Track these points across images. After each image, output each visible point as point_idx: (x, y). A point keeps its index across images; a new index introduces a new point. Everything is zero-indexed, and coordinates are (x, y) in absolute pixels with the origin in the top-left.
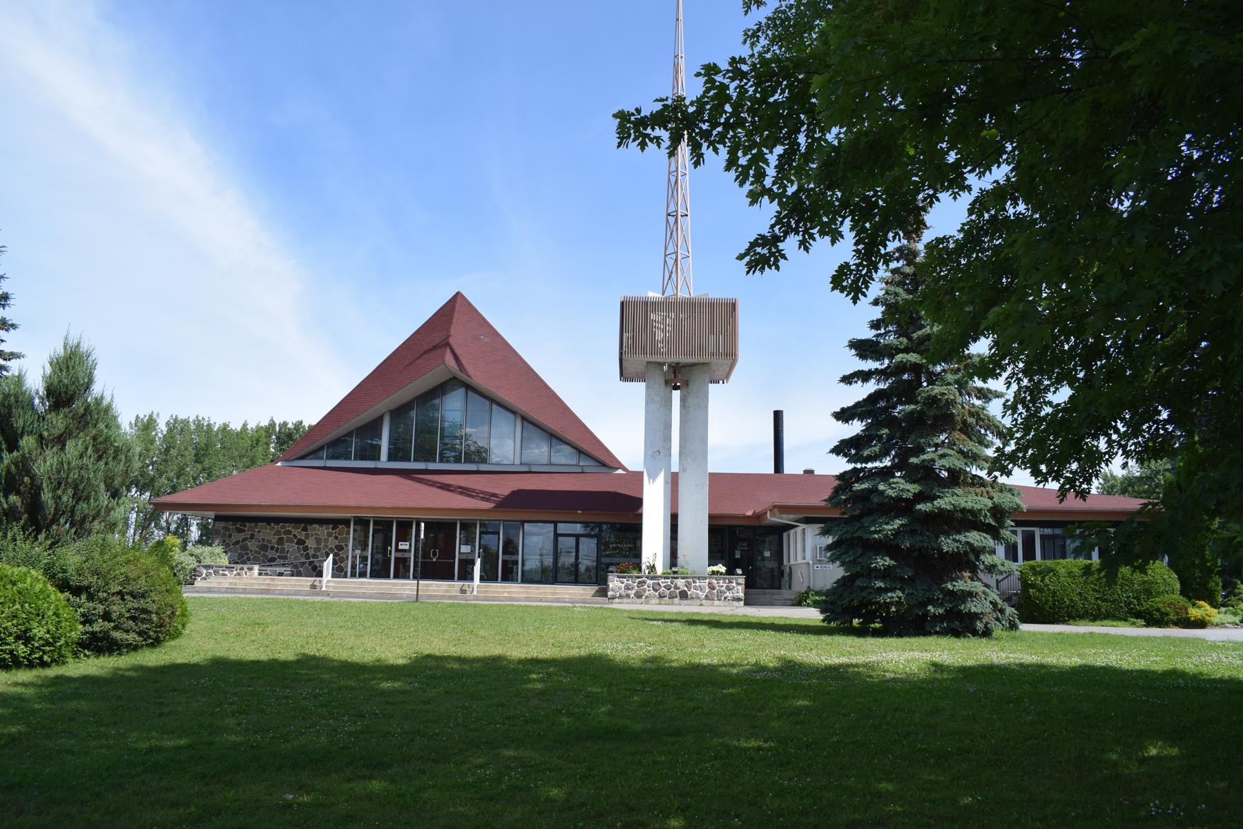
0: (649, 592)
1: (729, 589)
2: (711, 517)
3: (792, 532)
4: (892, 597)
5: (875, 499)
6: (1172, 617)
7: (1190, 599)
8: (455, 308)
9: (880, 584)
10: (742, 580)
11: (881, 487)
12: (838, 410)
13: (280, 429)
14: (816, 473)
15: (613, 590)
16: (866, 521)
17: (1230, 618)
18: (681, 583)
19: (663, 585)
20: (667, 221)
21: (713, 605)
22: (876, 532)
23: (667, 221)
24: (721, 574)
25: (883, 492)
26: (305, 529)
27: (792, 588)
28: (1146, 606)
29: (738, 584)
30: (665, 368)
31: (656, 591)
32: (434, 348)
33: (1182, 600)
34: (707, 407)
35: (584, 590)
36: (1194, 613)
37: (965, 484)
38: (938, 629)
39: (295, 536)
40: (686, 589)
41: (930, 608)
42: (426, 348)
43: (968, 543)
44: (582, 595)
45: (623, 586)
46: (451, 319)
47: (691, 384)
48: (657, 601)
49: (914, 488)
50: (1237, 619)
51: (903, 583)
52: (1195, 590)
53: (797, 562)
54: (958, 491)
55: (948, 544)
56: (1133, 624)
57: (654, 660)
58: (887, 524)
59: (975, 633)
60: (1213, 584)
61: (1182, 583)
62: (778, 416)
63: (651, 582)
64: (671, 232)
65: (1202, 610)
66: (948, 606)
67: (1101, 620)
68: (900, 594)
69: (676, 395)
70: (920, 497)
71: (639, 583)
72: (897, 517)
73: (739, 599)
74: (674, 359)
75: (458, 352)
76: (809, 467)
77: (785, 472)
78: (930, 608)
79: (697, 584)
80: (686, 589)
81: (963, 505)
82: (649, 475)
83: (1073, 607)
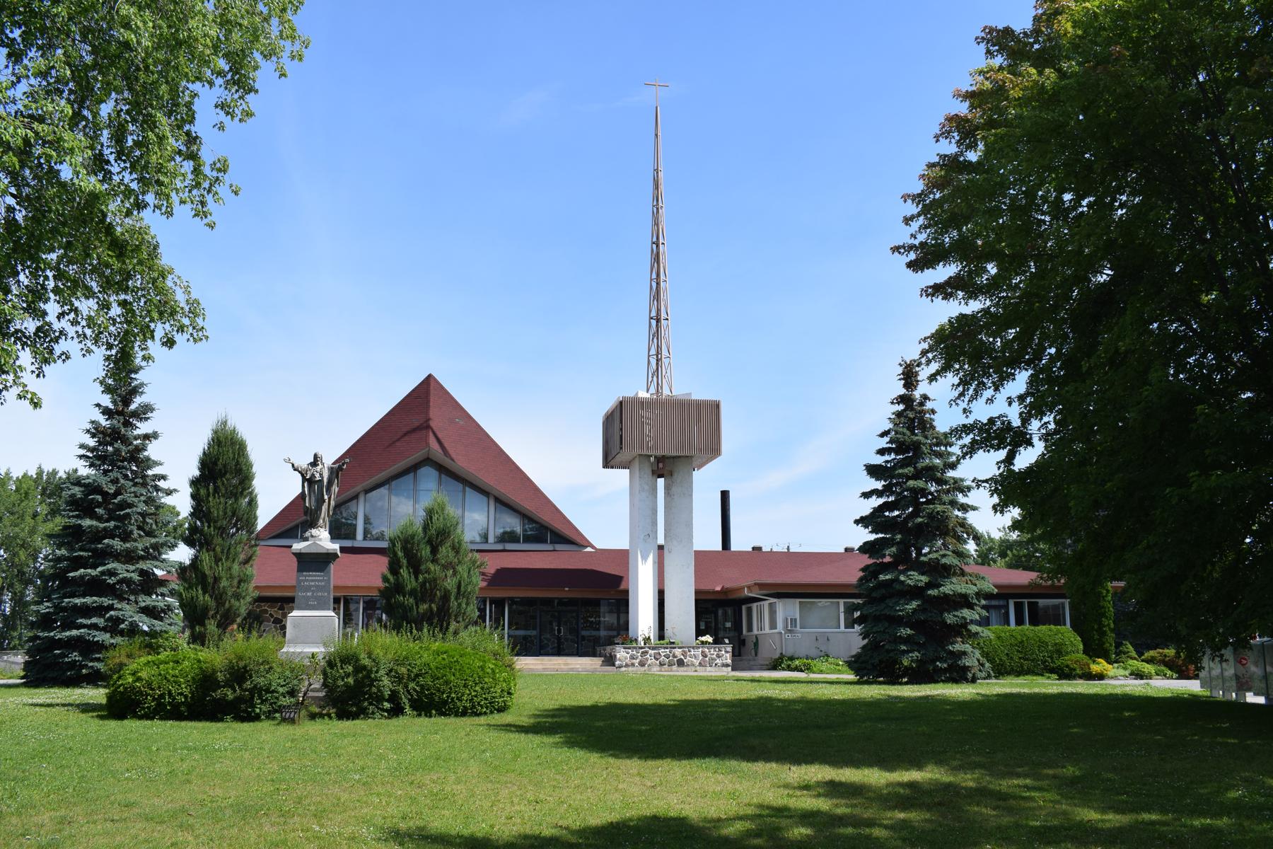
0: (651, 661)
1: (718, 656)
2: (697, 592)
3: (754, 606)
4: (912, 657)
5: (898, 587)
6: (1078, 672)
7: (1091, 657)
8: (427, 392)
9: (904, 648)
10: (729, 649)
11: (902, 578)
12: (858, 518)
13: (49, 478)
14: (764, 550)
15: (620, 660)
16: (890, 602)
17: (1122, 672)
18: (678, 652)
19: (663, 654)
20: (650, 322)
21: (705, 671)
22: (900, 610)
23: (650, 322)
24: (709, 643)
25: (903, 582)
26: (282, 608)
27: (759, 655)
28: (1058, 663)
29: (727, 652)
30: (652, 459)
31: (657, 659)
32: (414, 430)
33: (1085, 658)
34: (692, 495)
35: (592, 660)
36: (1095, 668)
37: (955, 574)
38: (943, 678)
39: (271, 615)
40: (682, 657)
41: (938, 663)
42: (405, 430)
43: (963, 617)
44: (591, 665)
45: (628, 656)
46: (428, 402)
47: (675, 475)
48: (658, 668)
49: (924, 579)
50: (1127, 673)
51: (919, 647)
52: (1095, 649)
53: (763, 632)
54: (954, 580)
55: (950, 618)
56: (1049, 678)
57: (802, 697)
58: (907, 604)
59: (967, 681)
60: (1108, 645)
61: (1085, 645)
62: (725, 496)
63: (653, 652)
64: (656, 334)
65: (1100, 666)
66: (950, 662)
67: (1024, 675)
68: (917, 654)
69: (661, 482)
70: (930, 585)
71: (642, 653)
72: (912, 599)
73: (727, 665)
74: (660, 453)
75: (440, 435)
76: (757, 544)
77: (732, 549)
78: (938, 663)
79: (692, 653)
80: (682, 657)
81: (959, 591)
82: (642, 557)
83: (1002, 665)
